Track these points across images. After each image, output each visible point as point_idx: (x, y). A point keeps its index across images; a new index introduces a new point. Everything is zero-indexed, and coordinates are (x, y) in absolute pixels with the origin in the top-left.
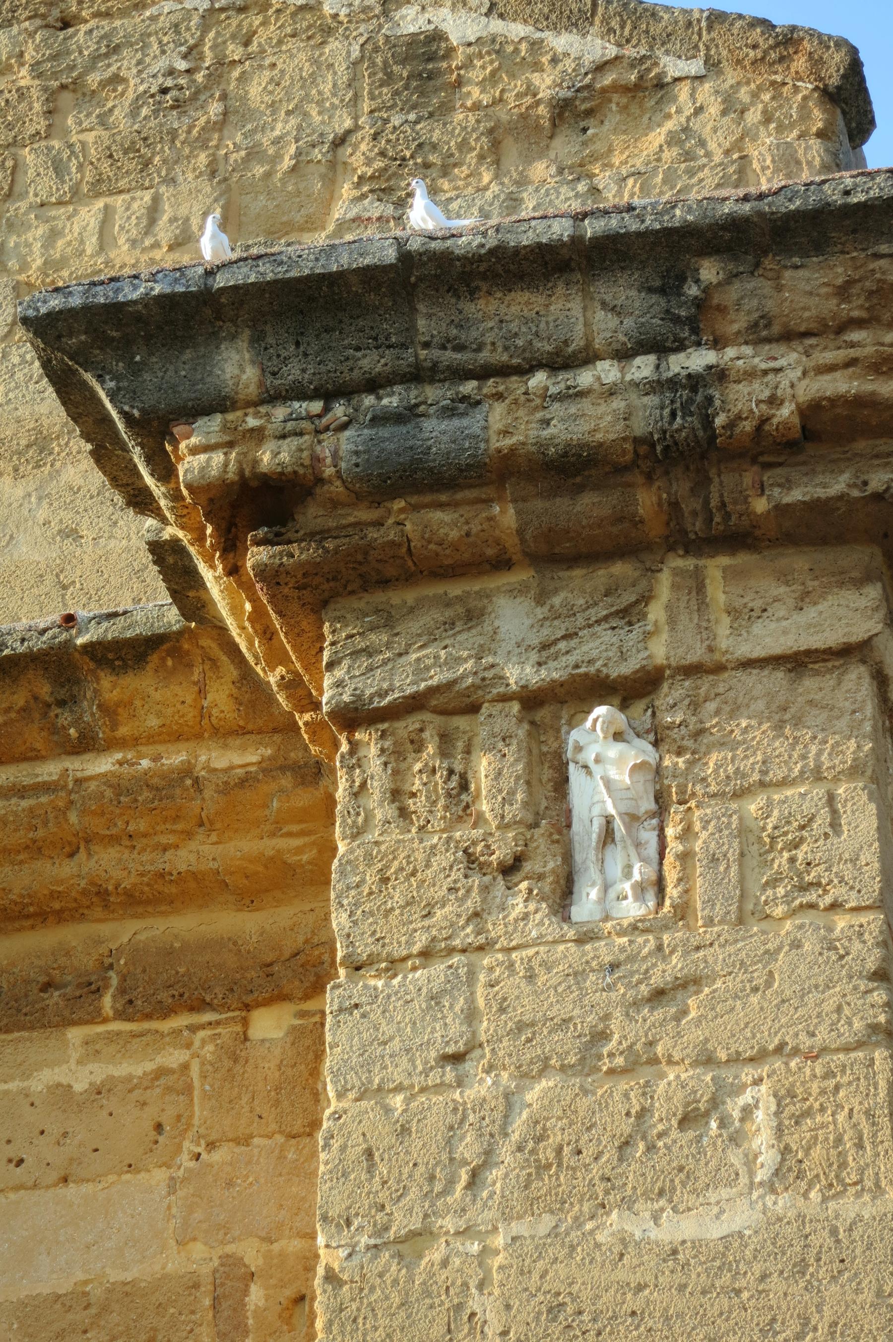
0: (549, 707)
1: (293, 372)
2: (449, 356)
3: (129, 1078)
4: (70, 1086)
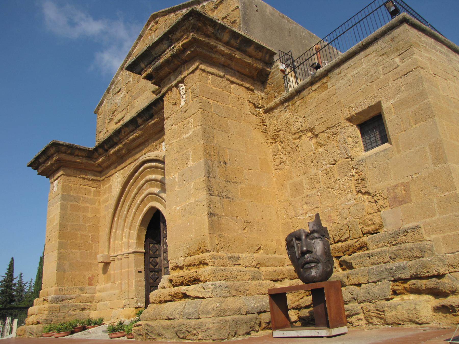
0: (177, 86)
1: (146, 63)
2: (156, 56)
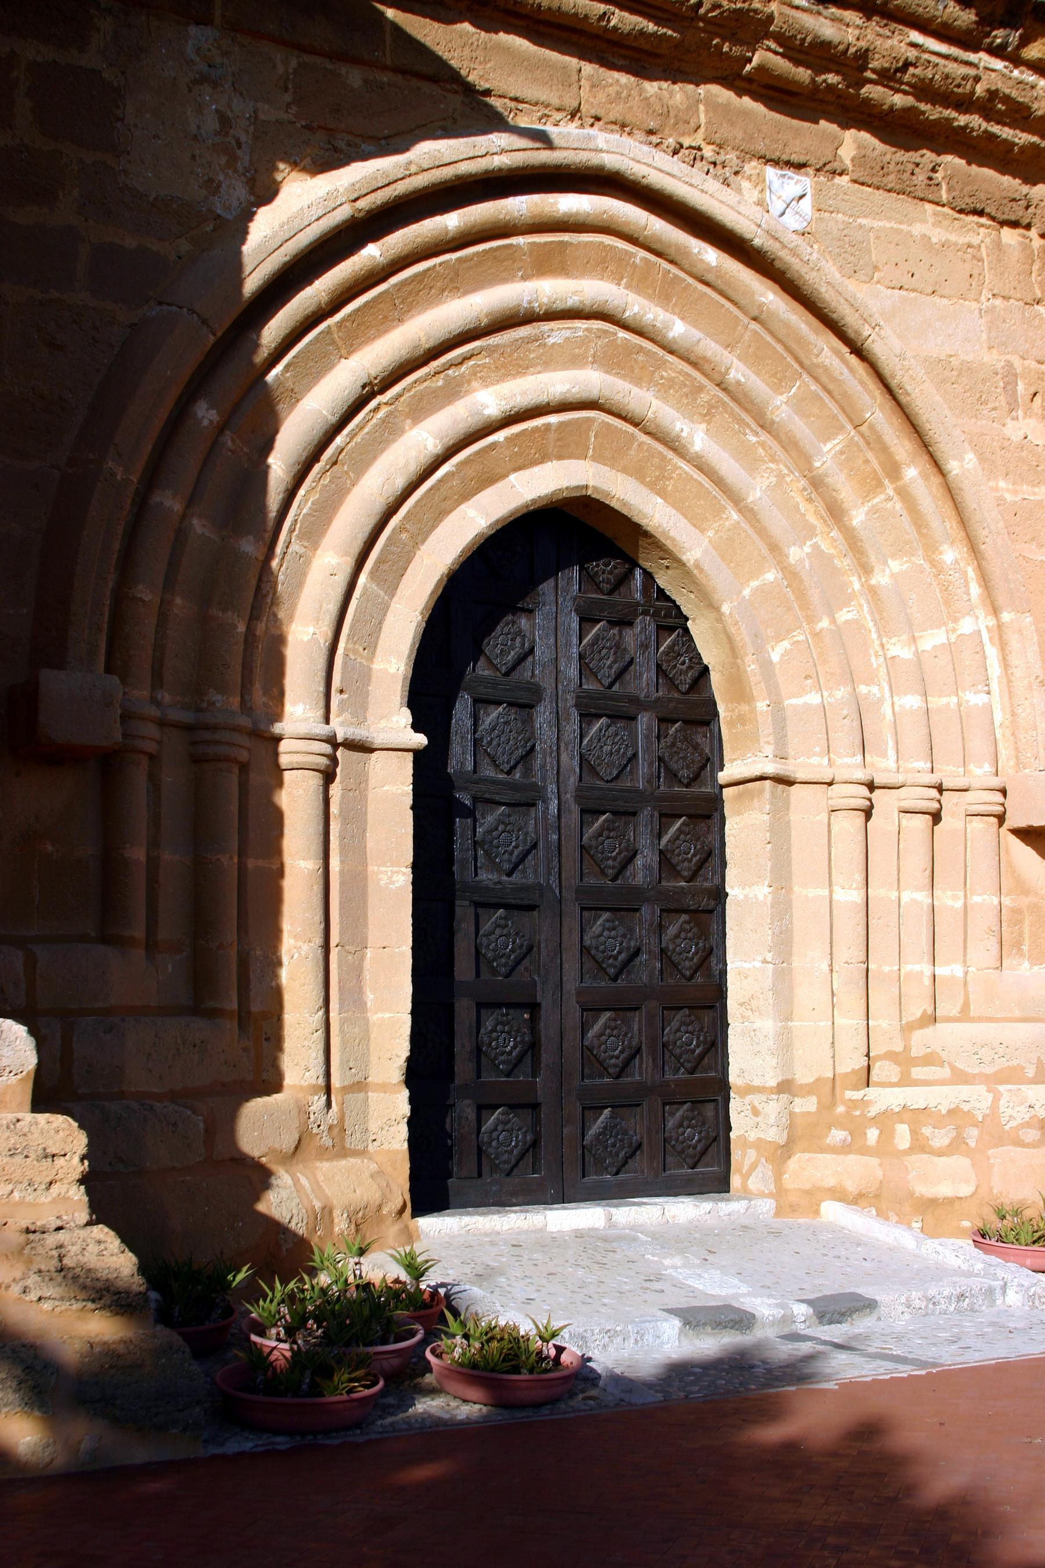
3: (956, 244)
4: (930, 238)
